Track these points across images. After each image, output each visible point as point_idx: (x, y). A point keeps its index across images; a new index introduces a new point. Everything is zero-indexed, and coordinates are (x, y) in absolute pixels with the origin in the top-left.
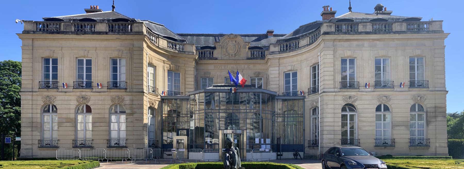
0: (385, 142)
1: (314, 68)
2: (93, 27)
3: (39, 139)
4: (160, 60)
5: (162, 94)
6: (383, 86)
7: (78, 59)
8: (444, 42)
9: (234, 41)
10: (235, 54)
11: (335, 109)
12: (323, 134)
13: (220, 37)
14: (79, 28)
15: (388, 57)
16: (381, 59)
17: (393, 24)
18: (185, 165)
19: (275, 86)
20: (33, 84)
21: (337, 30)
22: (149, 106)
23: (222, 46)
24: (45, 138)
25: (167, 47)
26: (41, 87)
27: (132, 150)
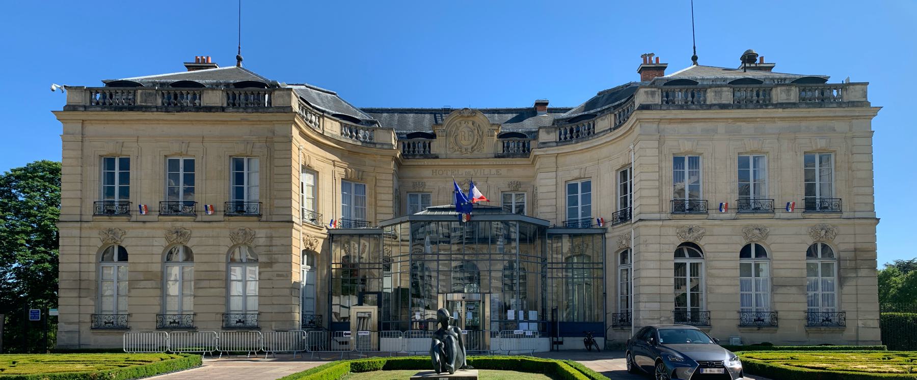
0: (759, 318)
1: (624, 175)
2: (198, 97)
3: (94, 312)
4: (327, 159)
5: (331, 226)
6: (754, 209)
7: (169, 160)
8: (871, 122)
9: (470, 123)
10: (472, 148)
11: (663, 252)
12: (640, 302)
13: (445, 114)
14: (171, 100)
15: (764, 153)
16: (749, 157)
17: (772, 88)
18: (363, 363)
19: (549, 209)
20: (83, 206)
21: (664, 100)
22: (303, 248)
23: (448, 131)
24: (104, 311)
25: (340, 135)
26: (97, 213)
27: (269, 333)
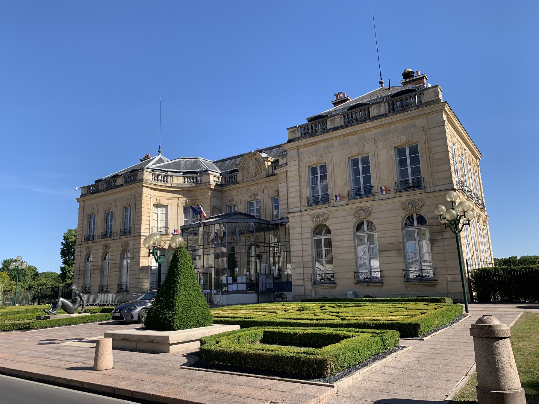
9: (254, 159)
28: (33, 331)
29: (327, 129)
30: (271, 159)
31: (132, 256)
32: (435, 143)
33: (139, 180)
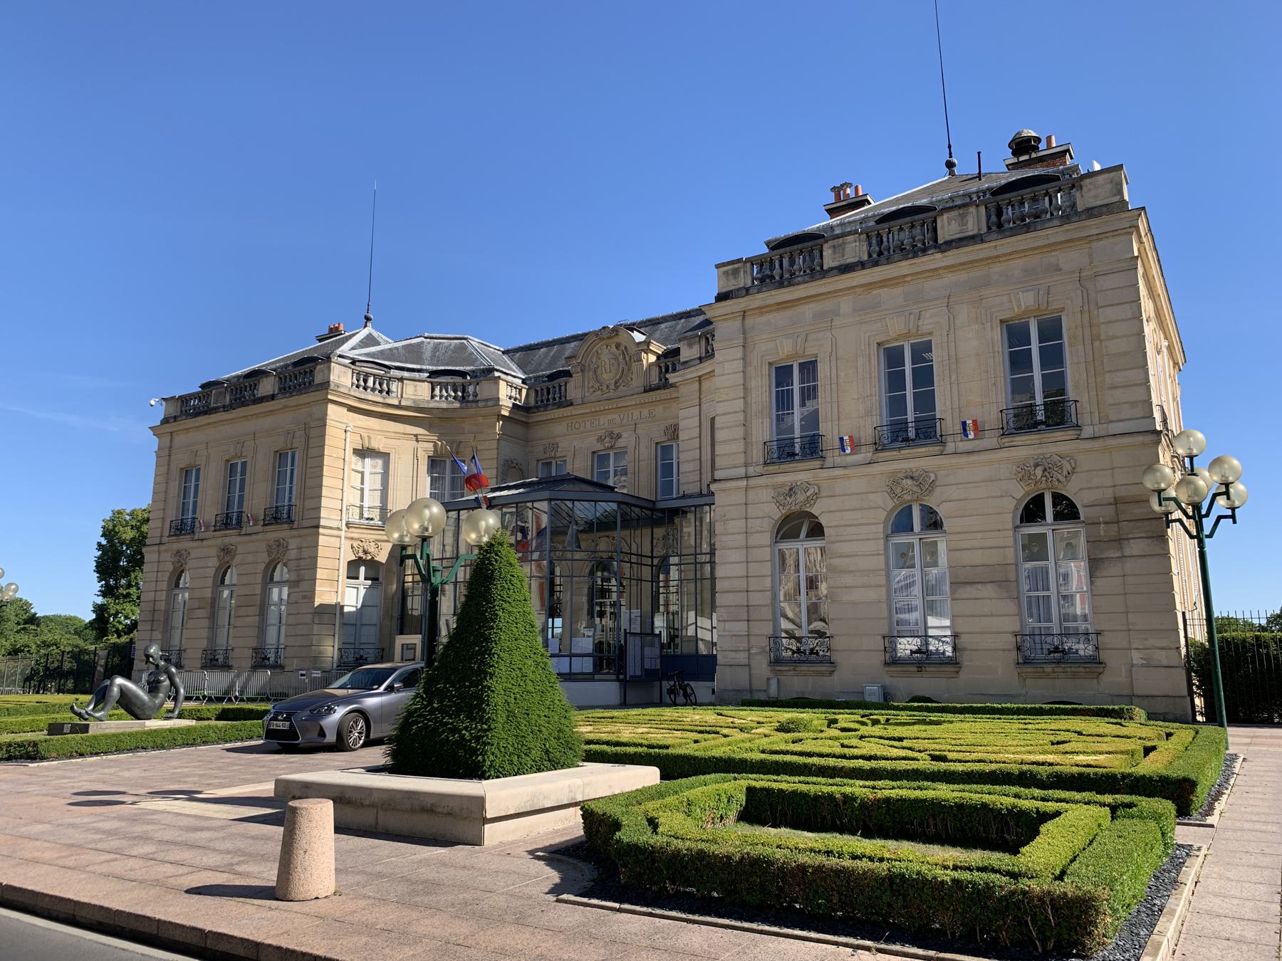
9: (613, 346)
10: (616, 383)
28: (45, 764)
29: (822, 267)
30: (658, 348)
31: (293, 577)
32: (1109, 313)
33: (318, 385)
